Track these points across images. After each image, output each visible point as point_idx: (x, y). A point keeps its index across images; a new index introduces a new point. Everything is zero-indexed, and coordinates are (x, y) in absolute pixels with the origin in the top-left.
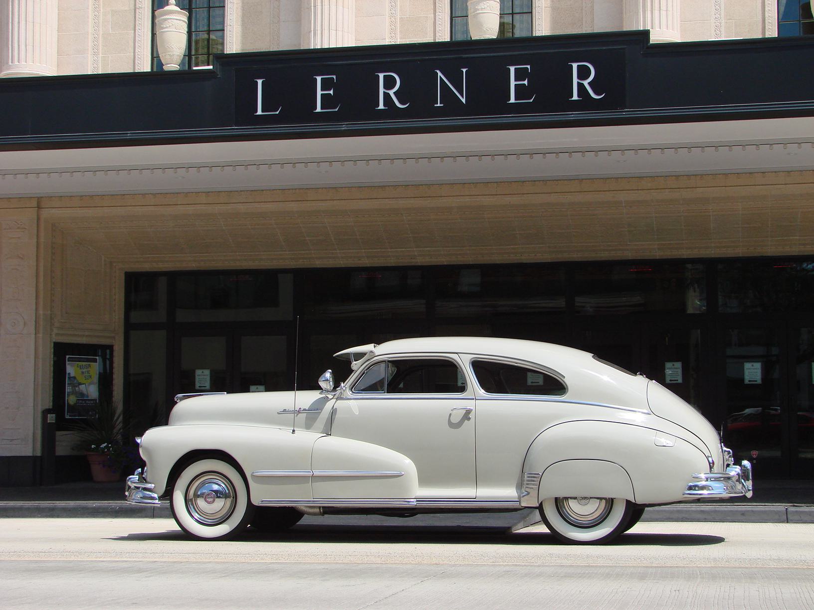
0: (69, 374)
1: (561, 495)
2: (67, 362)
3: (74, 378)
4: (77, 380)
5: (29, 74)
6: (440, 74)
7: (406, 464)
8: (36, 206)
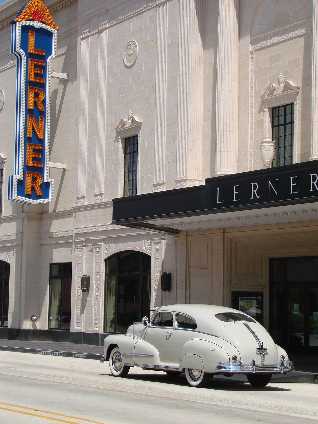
0: (240, 305)
1: (190, 368)
2: (239, 300)
3: (243, 307)
4: (245, 308)
5: (222, 174)
6: (270, 182)
7: (156, 352)
8: (223, 232)
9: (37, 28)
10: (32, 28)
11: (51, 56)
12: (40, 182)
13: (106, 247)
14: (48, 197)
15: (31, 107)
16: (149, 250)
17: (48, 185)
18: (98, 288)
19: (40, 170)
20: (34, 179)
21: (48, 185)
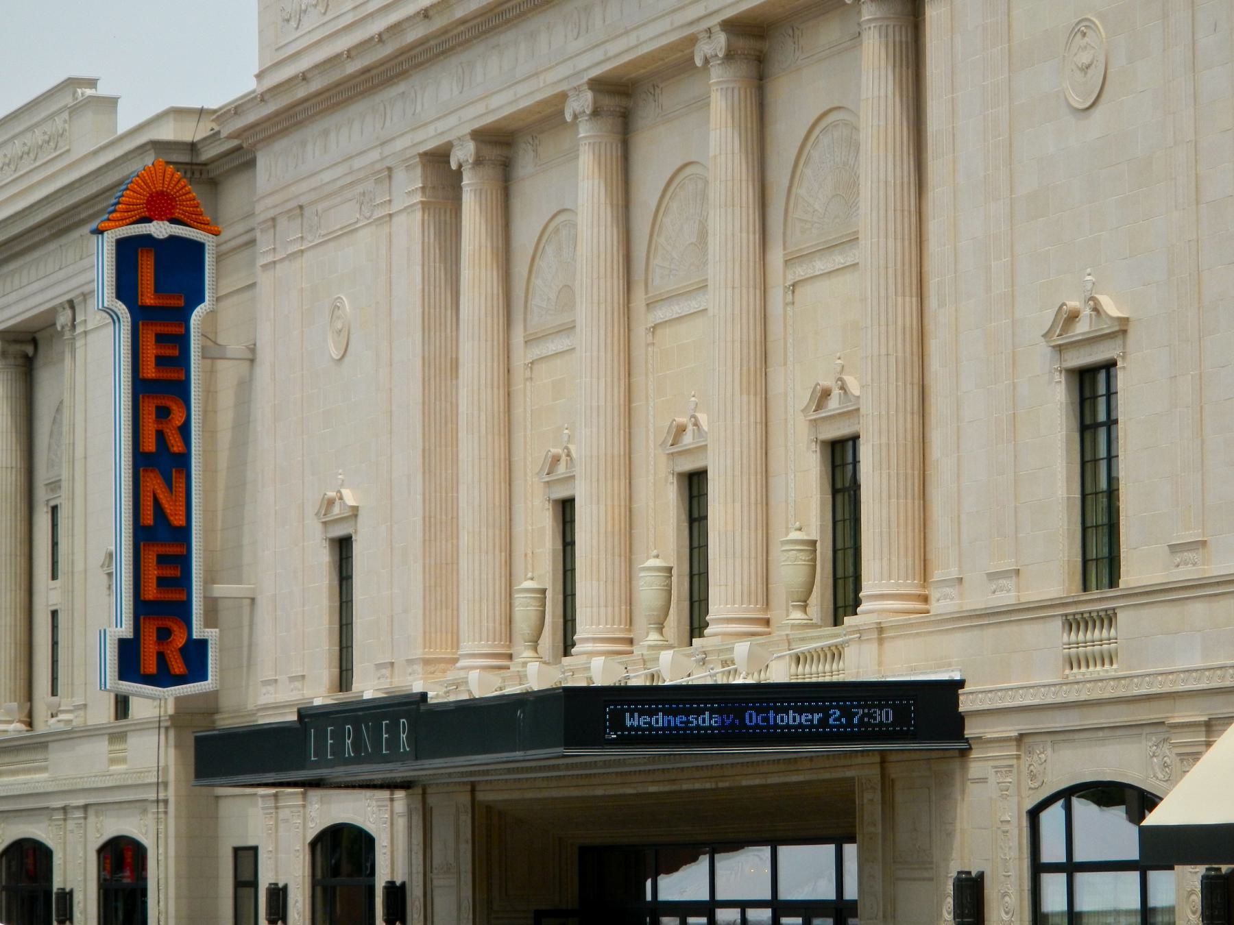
9: (161, 237)
10: (148, 239)
11: (202, 305)
12: (180, 641)
13: (1030, 765)
14: (206, 679)
15: (150, 445)
16: (1167, 781)
17: (203, 644)
18: (1011, 914)
19: (183, 611)
20: (164, 635)
21: (203, 644)
